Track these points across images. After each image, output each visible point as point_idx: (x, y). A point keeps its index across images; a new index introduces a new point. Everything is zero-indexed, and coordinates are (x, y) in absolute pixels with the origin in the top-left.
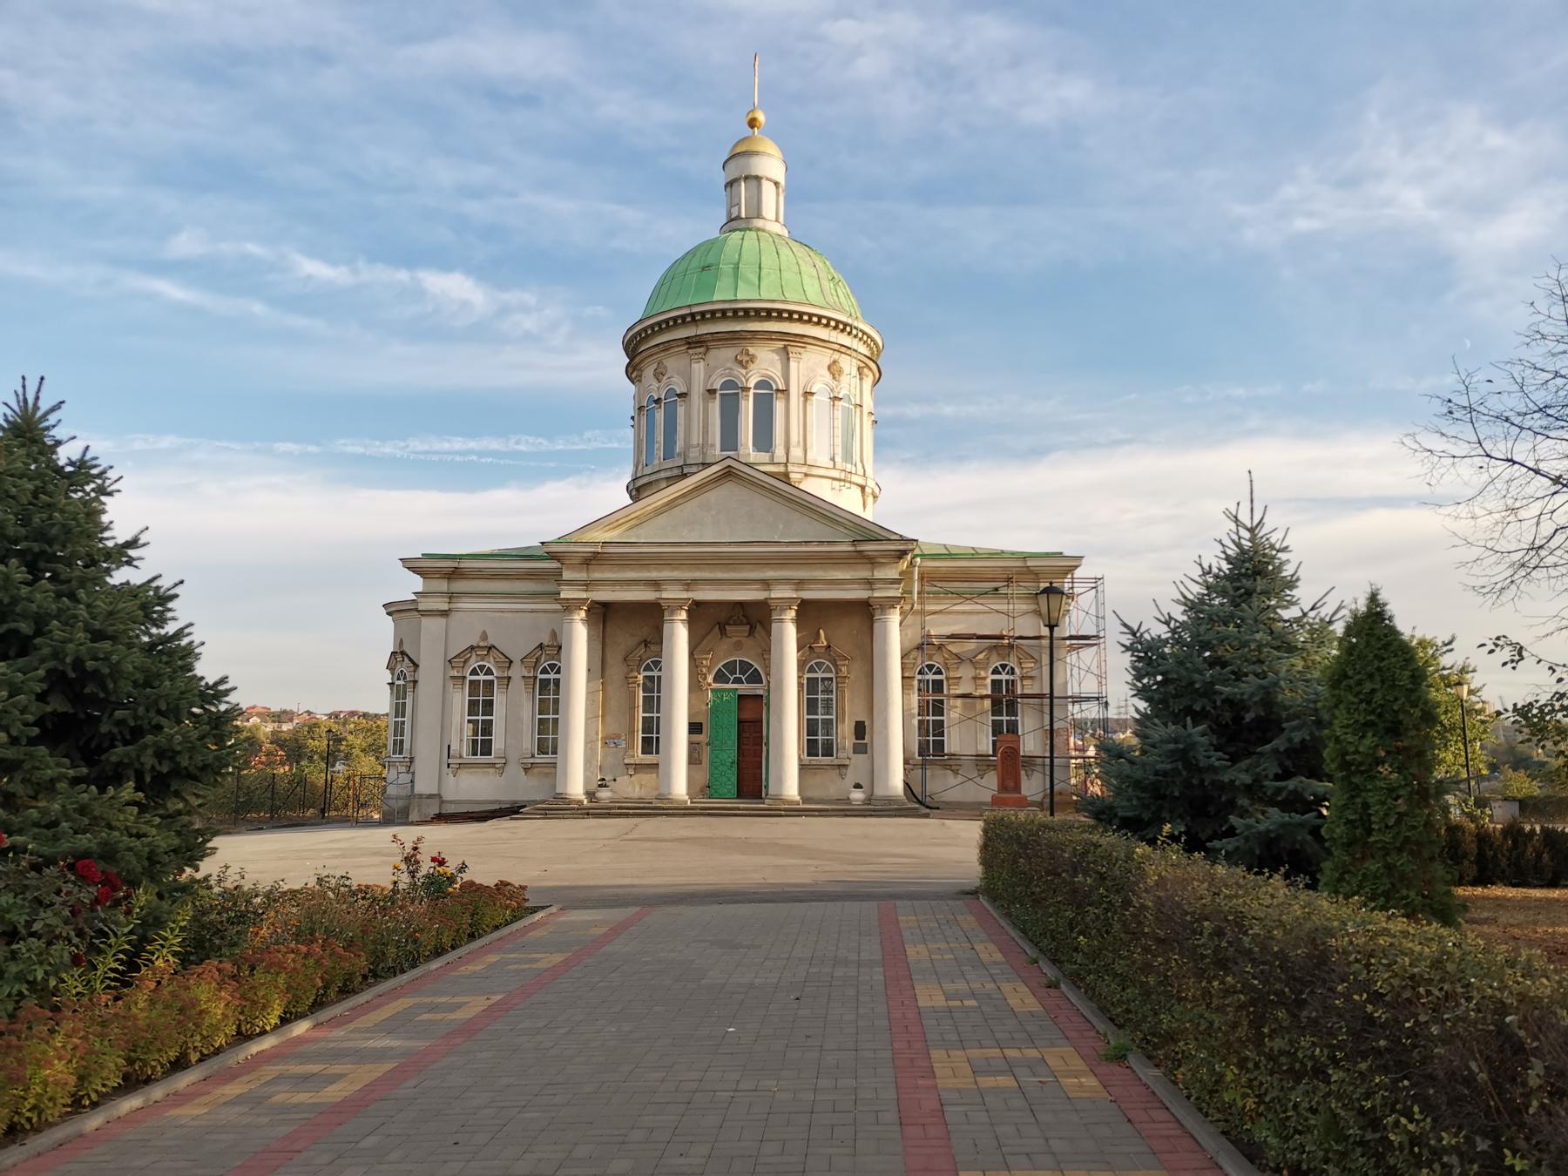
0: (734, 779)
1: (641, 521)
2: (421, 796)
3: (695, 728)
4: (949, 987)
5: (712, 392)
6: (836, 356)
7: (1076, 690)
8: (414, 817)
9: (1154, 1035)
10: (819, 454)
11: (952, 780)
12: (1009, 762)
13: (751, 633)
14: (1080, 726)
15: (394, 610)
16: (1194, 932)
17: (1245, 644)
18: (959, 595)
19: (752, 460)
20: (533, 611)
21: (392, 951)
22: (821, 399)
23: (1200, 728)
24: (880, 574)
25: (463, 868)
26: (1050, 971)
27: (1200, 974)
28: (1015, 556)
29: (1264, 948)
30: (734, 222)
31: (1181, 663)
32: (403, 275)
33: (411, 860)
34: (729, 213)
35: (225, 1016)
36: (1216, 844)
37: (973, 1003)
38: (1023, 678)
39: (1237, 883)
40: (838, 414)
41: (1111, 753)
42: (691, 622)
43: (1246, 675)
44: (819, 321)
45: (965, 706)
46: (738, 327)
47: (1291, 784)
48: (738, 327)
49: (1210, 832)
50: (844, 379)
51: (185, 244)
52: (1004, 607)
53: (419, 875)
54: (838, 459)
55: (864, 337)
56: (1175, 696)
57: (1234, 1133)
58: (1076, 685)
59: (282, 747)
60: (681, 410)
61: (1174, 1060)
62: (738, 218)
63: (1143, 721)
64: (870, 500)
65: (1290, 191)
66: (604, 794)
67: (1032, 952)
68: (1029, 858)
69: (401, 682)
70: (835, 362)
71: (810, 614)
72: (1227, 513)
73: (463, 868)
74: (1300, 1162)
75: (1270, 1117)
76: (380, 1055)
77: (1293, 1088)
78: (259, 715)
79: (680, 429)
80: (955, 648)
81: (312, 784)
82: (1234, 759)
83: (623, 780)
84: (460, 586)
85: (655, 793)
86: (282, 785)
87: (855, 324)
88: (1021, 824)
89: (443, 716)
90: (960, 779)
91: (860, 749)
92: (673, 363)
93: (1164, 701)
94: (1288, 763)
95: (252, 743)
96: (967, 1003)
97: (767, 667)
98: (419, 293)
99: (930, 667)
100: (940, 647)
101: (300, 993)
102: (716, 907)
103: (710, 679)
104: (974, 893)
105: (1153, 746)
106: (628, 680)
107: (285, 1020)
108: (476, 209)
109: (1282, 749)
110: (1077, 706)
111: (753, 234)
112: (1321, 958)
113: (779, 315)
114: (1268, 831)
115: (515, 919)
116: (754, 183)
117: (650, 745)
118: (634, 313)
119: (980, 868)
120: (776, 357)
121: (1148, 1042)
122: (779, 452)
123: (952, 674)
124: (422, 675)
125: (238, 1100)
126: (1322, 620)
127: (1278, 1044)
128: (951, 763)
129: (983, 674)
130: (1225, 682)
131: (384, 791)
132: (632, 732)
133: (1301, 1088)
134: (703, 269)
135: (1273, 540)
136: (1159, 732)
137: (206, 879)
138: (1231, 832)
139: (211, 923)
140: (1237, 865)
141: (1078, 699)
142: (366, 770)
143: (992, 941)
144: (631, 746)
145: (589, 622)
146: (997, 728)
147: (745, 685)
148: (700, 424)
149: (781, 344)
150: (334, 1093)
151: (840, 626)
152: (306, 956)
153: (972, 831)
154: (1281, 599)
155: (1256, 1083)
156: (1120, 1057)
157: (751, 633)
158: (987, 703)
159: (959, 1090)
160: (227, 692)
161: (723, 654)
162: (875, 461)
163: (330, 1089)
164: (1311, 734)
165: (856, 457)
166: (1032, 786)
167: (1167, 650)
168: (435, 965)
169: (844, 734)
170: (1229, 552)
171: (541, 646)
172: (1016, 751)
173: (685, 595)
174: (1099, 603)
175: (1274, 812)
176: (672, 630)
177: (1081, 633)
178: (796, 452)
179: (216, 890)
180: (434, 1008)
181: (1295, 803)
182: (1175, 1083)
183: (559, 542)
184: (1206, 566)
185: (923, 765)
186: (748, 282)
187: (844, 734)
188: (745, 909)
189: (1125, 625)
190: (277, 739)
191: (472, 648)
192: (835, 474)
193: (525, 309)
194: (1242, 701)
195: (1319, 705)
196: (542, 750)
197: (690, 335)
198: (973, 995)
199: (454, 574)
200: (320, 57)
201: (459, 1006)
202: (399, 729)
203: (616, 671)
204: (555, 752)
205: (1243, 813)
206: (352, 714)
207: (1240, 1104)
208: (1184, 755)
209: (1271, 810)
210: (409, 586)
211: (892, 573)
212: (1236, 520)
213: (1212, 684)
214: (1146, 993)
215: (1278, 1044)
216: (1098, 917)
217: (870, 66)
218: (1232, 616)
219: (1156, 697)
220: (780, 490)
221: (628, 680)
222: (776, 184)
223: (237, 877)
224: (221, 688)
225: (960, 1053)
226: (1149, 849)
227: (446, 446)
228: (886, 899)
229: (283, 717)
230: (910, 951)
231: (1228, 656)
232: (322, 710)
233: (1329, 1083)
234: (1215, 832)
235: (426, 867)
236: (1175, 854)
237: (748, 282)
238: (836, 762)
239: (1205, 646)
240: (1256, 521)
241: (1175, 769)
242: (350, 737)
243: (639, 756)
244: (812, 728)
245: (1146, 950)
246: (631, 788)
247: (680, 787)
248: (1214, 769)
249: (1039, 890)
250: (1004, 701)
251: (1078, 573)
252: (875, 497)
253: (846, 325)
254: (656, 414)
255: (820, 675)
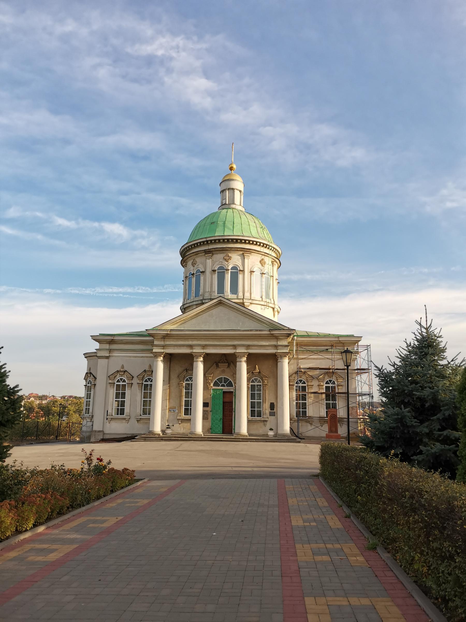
0: (221, 426)
1: (185, 322)
2: (95, 431)
3: (205, 405)
4: (305, 517)
5: (214, 271)
6: (263, 257)
7: (360, 391)
8: (92, 440)
9: (387, 539)
10: (256, 295)
11: (310, 427)
12: (332, 420)
13: (229, 366)
14: (363, 405)
15: (88, 356)
16: (403, 496)
17: (425, 375)
18: (312, 352)
19: (229, 298)
20: (142, 357)
21: (79, 497)
22: (257, 274)
23: (407, 409)
24: (280, 343)
25: (109, 463)
26: (347, 510)
27: (405, 514)
28: (334, 336)
29: (430, 505)
30: (224, 206)
31: (399, 382)
32: (96, 224)
33: (89, 459)
34: (222, 202)
35: (11, 523)
36: (415, 457)
37: (314, 524)
38: (338, 386)
39: (421, 476)
40: (264, 280)
41: (373, 418)
42: (205, 362)
43: (426, 388)
44: (256, 243)
45: (315, 397)
46: (225, 246)
47: (445, 433)
48: (225, 246)
49: (412, 452)
50: (266, 266)
51: (12, 213)
52: (330, 357)
53: (92, 465)
54: (264, 297)
55: (274, 250)
56: (397, 396)
57: (419, 582)
58: (360, 388)
59: (42, 410)
60: (202, 278)
61: (395, 550)
62: (225, 204)
63: (383, 404)
64: (276, 313)
65: (444, 192)
66: (169, 431)
67: (340, 503)
68: (338, 462)
69: (89, 385)
70: (262, 259)
71: (253, 359)
72: (416, 322)
73: (109, 463)
74: (445, 596)
75: (433, 575)
76: (72, 541)
77: (441, 564)
78: (34, 397)
79: (202, 285)
80: (311, 373)
81: (53, 426)
82: (422, 422)
83: (177, 426)
84: (114, 347)
85: (189, 431)
86: (41, 426)
87: (271, 245)
88: (336, 448)
89: (106, 399)
90: (313, 427)
91: (273, 414)
92: (199, 260)
93: (393, 398)
94: (444, 424)
95: (30, 409)
96: (312, 524)
97: (235, 380)
98: (101, 231)
99: (301, 381)
100: (305, 373)
101: (42, 514)
102: (211, 481)
103: (212, 385)
104: (317, 476)
105: (389, 417)
106: (179, 385)
107: (35, 526)
108: (124, 199)
109: (441, 418)
110: (360, 398)
111: (231, 210)
112: (451, 509)
113: (241, 241)
114: (436, 452)
115: (130, 484)
116: (232, 191)
117: (188, 411)
118: (184, 241)
119: (319, 466)
120: (239, 257)
121: (385, 542)
122: (240, 295)
123: (309, 384)
124: (98, 382)
125: (14, 559)
126: (456, 365)
127: (435, 545)
128: (309, 420)
129: (322, 384)
130: (417, 391)
131: (81, 429)
132: (180, 406)
133: (445, 563)
134: (212, 223)
135: (435, 333)
136: (391, 411)
137: (7, 466)
138: (421, 453)
139: (7, 484)
140: (421, 468)
141: (361, 395)
142: (74, 420)
143: (324, 497)
144: (180, 412)
145: (164, 361)
146: (328, 406)
147: (226, 388)
148: (210, 283)
149: (241, 252)
150: (52, 557)
151: (265, 364)
152: (44, 499)
153: (316, 449)
154: (439, 357)
155: (427, 561)
156: (374, 548)
157: (229, 366)
158: (324, 396)
159: (306, 562)
160: (18, 391)
161: (218, 375)
162: (278, 297)
163: (51, 555)
164: (453, 412)
165: (271, 297)
166: (342, 430)
167: (393, 377)
168: (96, 503)
169: (266, 408)
170: (418, 337)
171: (145, 371)
172: (336, 416)
173: (202, 351)
174: (369, 355)
175: (438, 444)
176: (197, 364)
177: (361, 368)
178: (247, 295)
179: (10, 471)
180: (95, 522)
181: (447, 441)
182: (396, 560)
183: (153, 329)
184: (409, 343)
185: (298, 421)
186: (229, 229)
187: (266, 408)
188: (223, 481)
189: (376, 367)
190: (41, 407)
191: (118, 371)
192: (262, 303)
193: (143, 237)
194: (424, 398)
195: (455, 401)
196: (145, 413)
197: (207, 249)
198: (315, 520)
199: (111, 342)
200: (67, 142)
201: (105, 521)
202: (88, 404)
203: (174, 381)
204: (149, 414)
205: (426, 445)
206: (70, 397)
207: (421, 570)
208: (401, 420)
209: (436, 443)
210: (94, 346)
211: (285, 343)
212: (420, 324)
213: (412, 391)
214: (385, 521)
215: (435, 545)
216: (365, 488)
217: (277, 145)
218: (419, 363)
219: (389, 396)
220: (241, 309)
221: (179, 385)
222: (240, 191)
223: (20, 465)
224: (16, 389)
225: (308, 545)
226: (385, 460)
227: (111, 290)
228: (281, 478)
229: (43, 398)
230: (290, 501)
231: (418, 380)
232: (58, 395)
233: (456, 562)
234: (414, 452)
235: (95, 462)
236: (396, 462)
237: (229, 229)
238: (263, 419)
239: (409, 375)
240: (428, 325)
241: (397, 426)
242: (69, 406)
243: (183, 416)
244: (253, 405)
245: (384, 503)
246: (179, 429)
247: (199, 429)
248: (412, 426)
249: (341, 474)
250: (331, 395)
251: (360, 343)
252: (278, 312)
253: (267, 245)
254: (192, 279)
255: (256, 384)
